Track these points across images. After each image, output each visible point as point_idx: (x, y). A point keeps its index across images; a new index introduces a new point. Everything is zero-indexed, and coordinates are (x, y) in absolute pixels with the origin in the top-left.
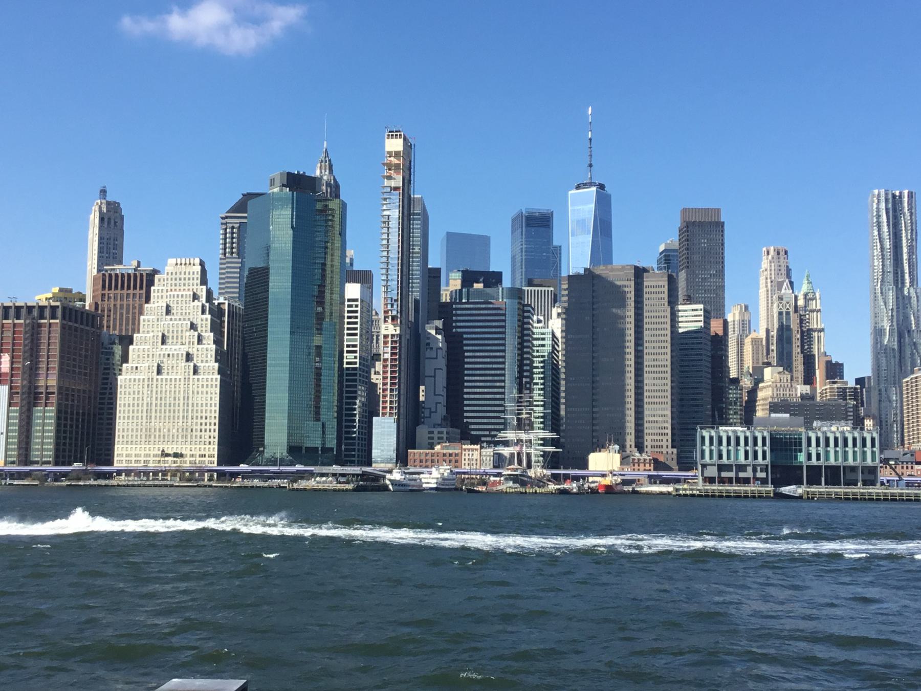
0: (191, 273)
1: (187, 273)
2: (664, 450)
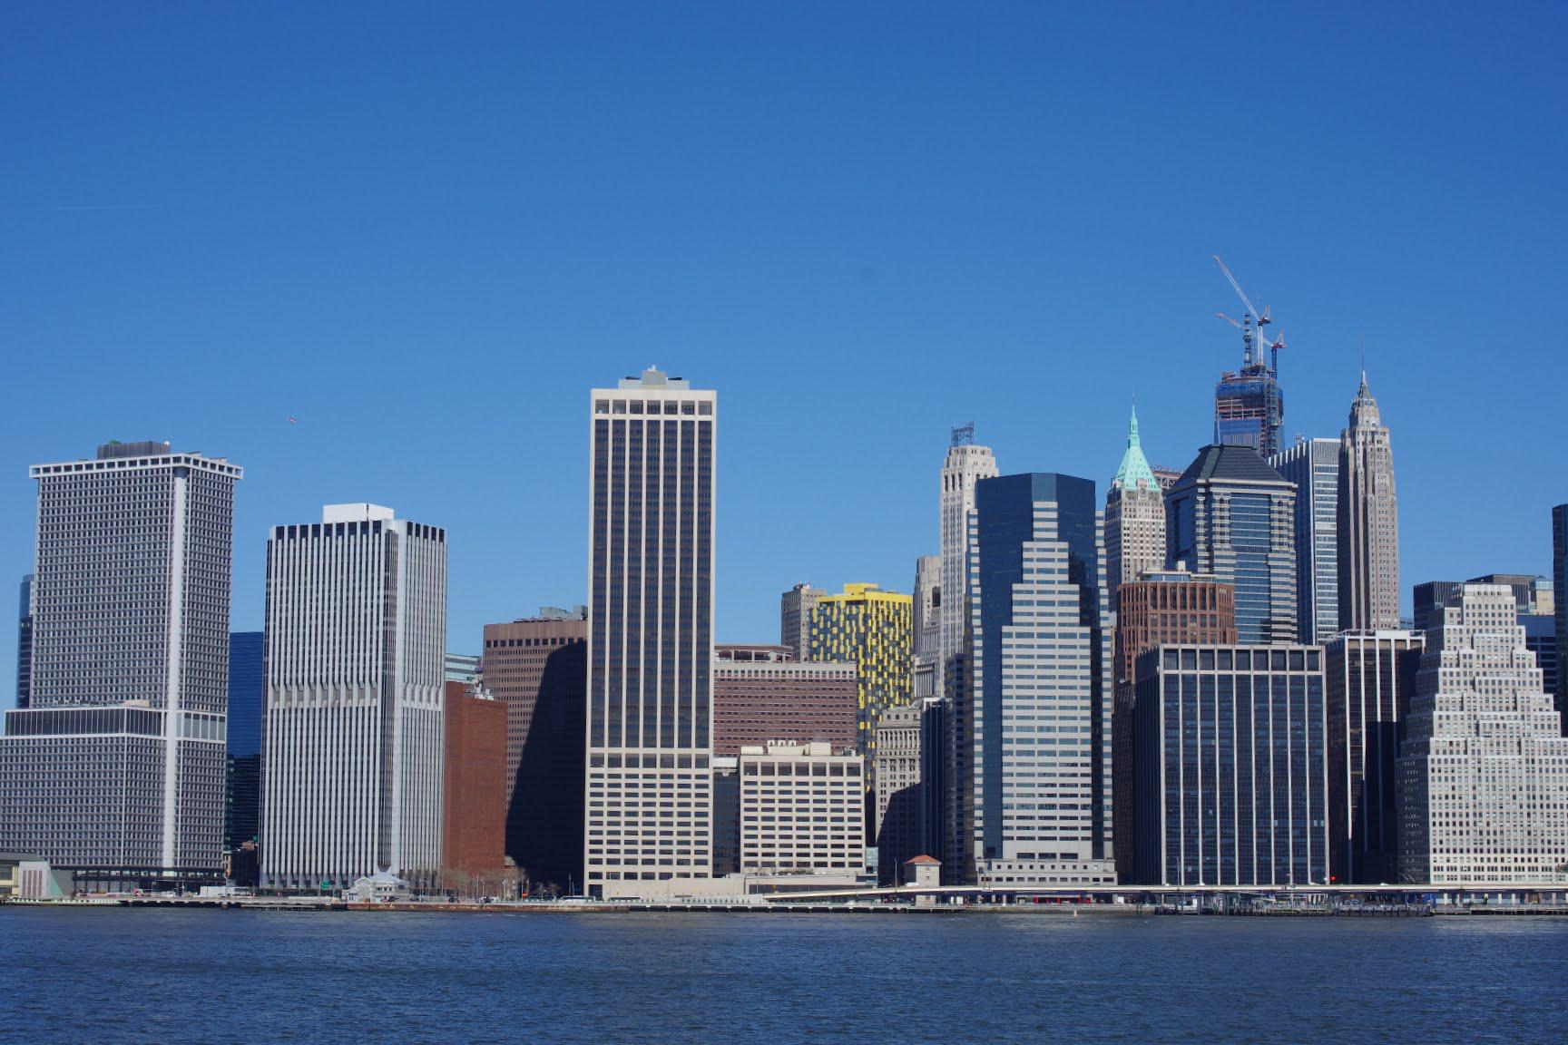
0: (1503, 607)
1: (1496, 607)
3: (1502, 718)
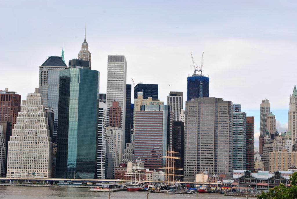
2: (226, 173)
3: (31, 131)
